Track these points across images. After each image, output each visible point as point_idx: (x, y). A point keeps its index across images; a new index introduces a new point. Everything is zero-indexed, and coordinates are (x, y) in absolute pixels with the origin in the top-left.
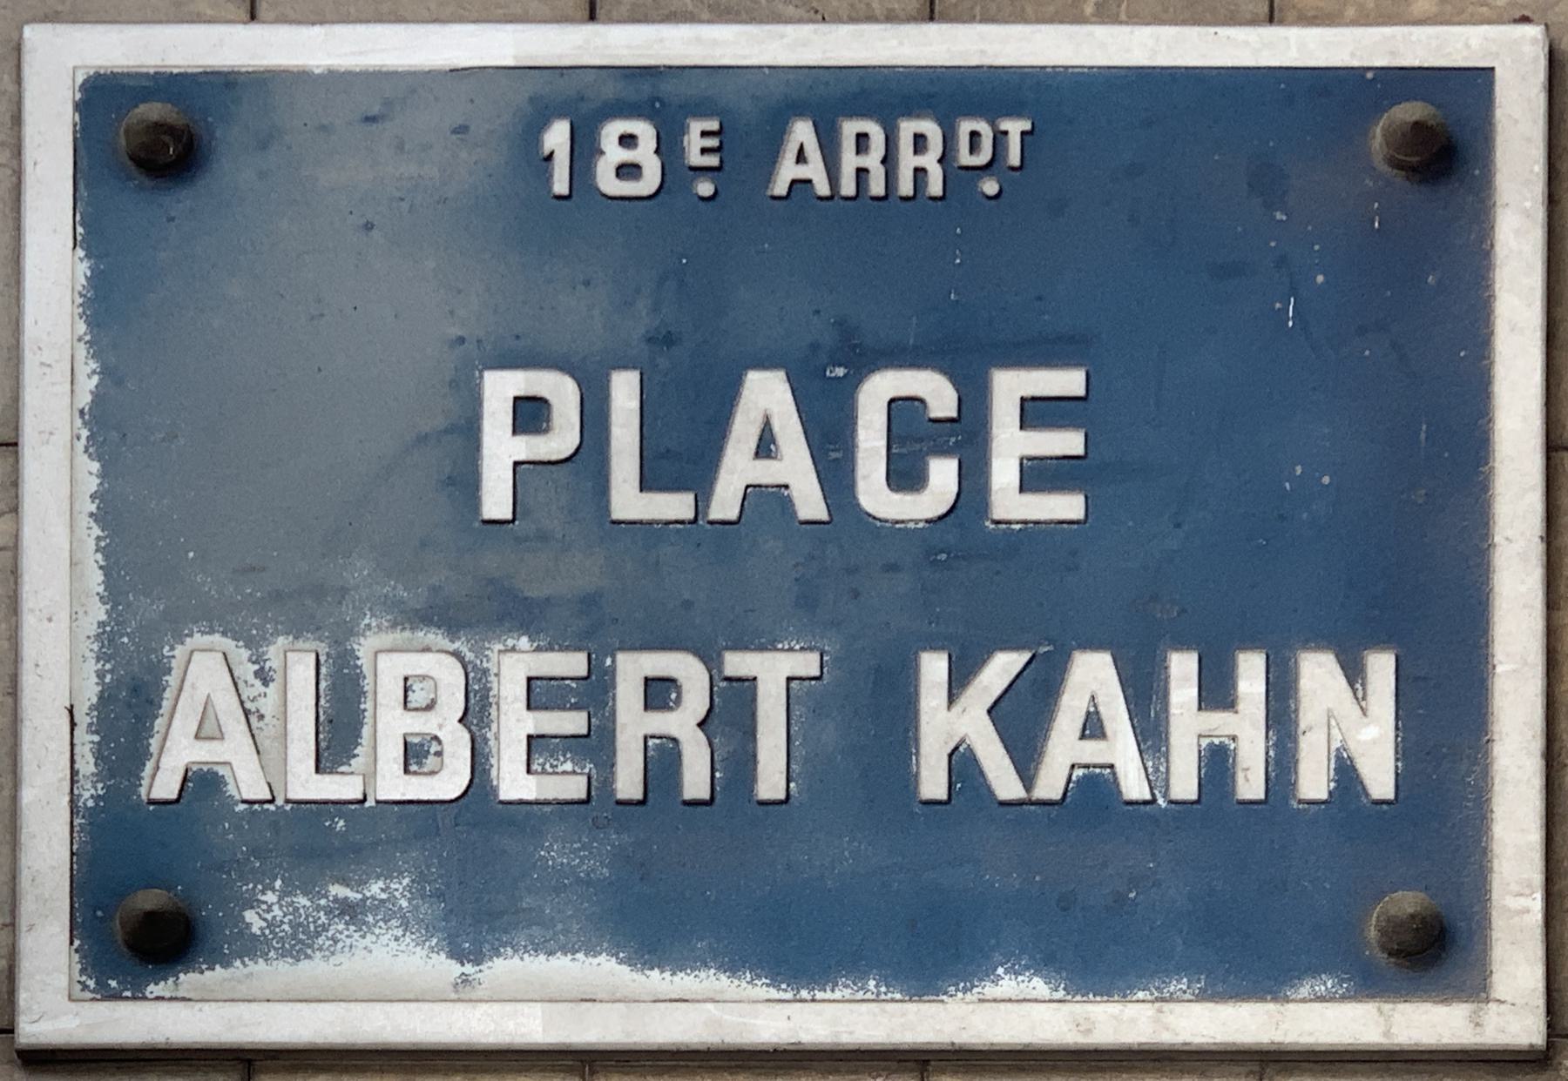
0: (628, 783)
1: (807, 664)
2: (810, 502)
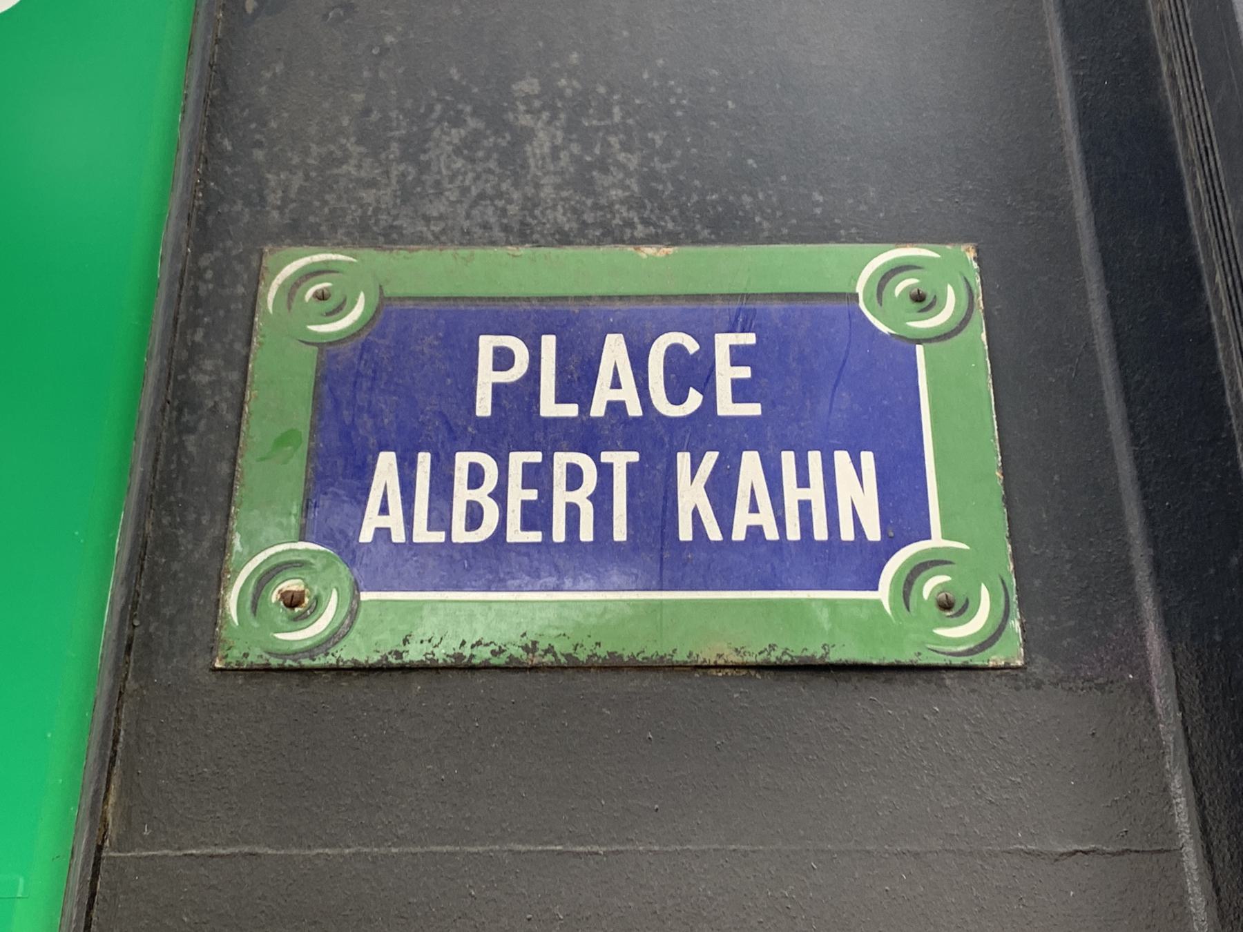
0: (559, 535)
1: (634, 457)
2: (634, 409)
